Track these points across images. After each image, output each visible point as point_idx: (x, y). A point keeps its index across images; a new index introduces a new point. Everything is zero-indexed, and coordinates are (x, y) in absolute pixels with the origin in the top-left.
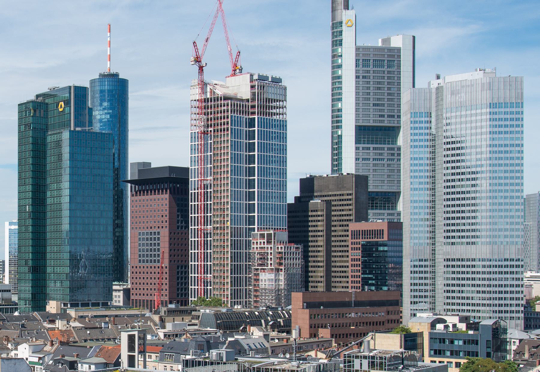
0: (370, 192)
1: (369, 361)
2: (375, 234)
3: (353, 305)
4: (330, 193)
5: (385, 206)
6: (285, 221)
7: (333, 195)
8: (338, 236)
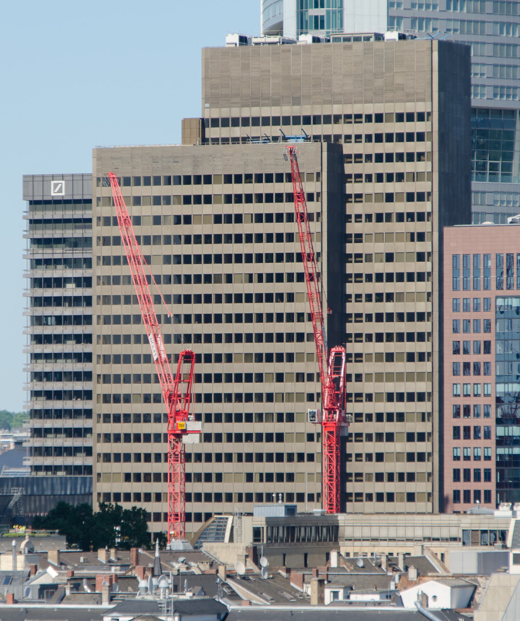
0: (475, 111)
4: (336, 110)
7: (348, 117)
8: (369, 278)
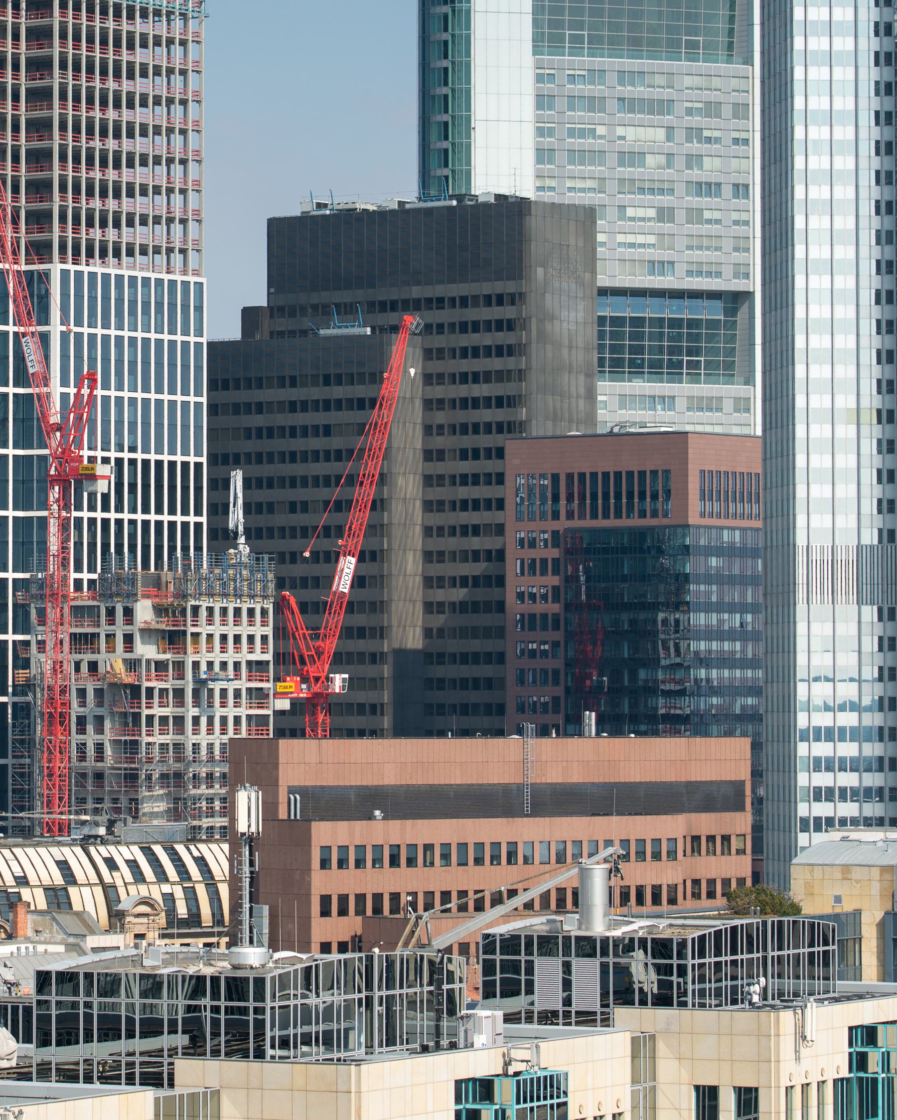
1: (604, 967)
2: (582, 497)
3: (528, 809)
4: (416, 292)
5: (680, 364)
6: (198, 428)
